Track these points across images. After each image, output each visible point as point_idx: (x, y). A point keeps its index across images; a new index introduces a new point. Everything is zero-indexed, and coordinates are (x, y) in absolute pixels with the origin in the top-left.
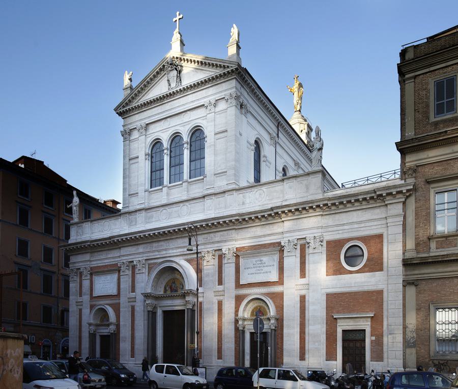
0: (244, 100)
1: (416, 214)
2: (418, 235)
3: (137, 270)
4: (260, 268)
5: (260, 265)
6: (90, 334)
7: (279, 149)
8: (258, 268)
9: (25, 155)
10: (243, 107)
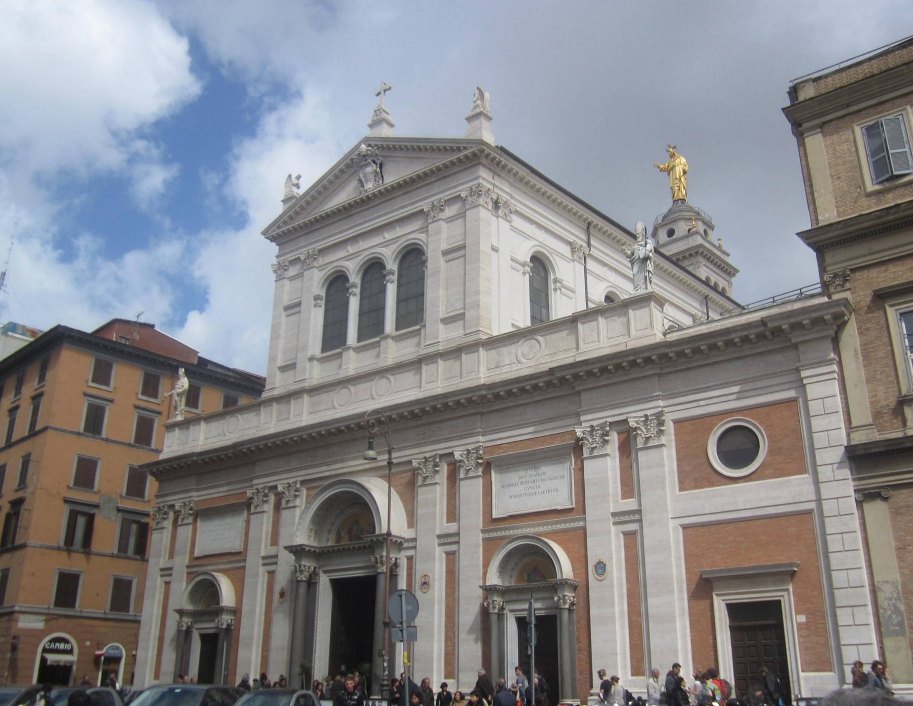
0: (500, 193)
1: (866, 357)
2: (876, 396)
3: (283, 502)
4: (535, 484)
5: (534, 478)
6: (179, 631)
7: (591, 264)
8: (530, 485)
9: (63, 324)
10: (501, 205)
